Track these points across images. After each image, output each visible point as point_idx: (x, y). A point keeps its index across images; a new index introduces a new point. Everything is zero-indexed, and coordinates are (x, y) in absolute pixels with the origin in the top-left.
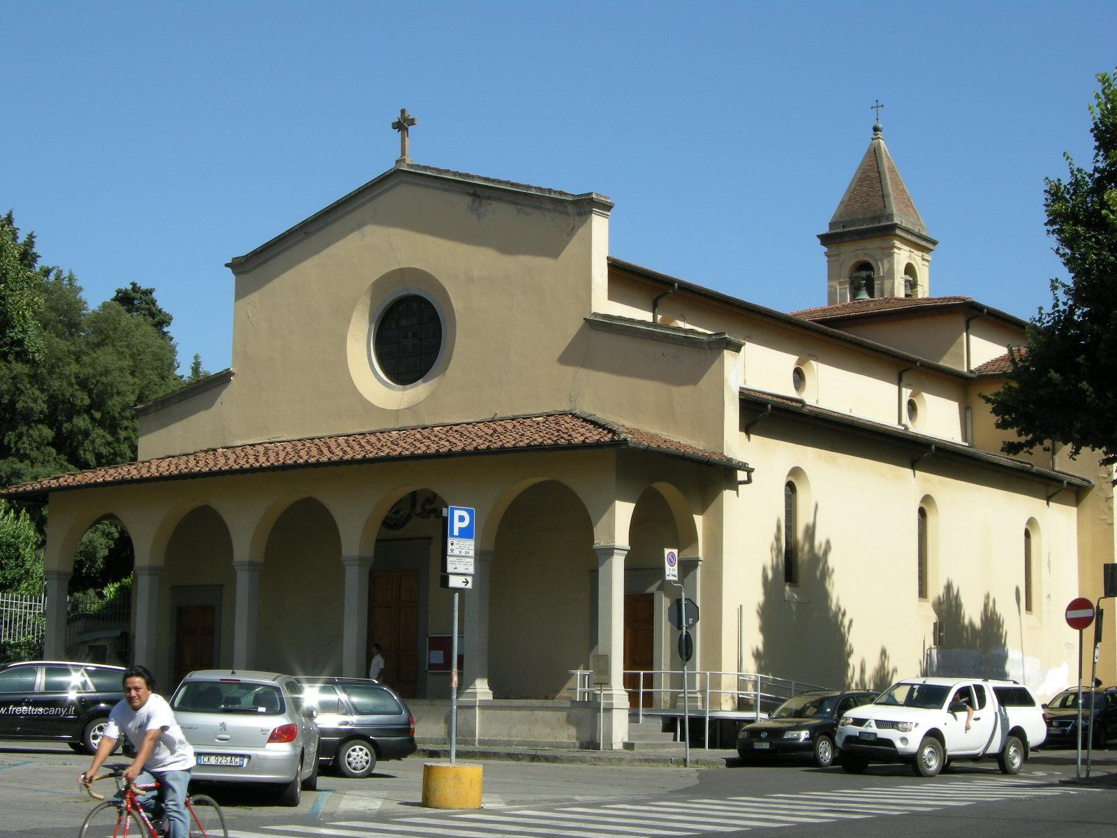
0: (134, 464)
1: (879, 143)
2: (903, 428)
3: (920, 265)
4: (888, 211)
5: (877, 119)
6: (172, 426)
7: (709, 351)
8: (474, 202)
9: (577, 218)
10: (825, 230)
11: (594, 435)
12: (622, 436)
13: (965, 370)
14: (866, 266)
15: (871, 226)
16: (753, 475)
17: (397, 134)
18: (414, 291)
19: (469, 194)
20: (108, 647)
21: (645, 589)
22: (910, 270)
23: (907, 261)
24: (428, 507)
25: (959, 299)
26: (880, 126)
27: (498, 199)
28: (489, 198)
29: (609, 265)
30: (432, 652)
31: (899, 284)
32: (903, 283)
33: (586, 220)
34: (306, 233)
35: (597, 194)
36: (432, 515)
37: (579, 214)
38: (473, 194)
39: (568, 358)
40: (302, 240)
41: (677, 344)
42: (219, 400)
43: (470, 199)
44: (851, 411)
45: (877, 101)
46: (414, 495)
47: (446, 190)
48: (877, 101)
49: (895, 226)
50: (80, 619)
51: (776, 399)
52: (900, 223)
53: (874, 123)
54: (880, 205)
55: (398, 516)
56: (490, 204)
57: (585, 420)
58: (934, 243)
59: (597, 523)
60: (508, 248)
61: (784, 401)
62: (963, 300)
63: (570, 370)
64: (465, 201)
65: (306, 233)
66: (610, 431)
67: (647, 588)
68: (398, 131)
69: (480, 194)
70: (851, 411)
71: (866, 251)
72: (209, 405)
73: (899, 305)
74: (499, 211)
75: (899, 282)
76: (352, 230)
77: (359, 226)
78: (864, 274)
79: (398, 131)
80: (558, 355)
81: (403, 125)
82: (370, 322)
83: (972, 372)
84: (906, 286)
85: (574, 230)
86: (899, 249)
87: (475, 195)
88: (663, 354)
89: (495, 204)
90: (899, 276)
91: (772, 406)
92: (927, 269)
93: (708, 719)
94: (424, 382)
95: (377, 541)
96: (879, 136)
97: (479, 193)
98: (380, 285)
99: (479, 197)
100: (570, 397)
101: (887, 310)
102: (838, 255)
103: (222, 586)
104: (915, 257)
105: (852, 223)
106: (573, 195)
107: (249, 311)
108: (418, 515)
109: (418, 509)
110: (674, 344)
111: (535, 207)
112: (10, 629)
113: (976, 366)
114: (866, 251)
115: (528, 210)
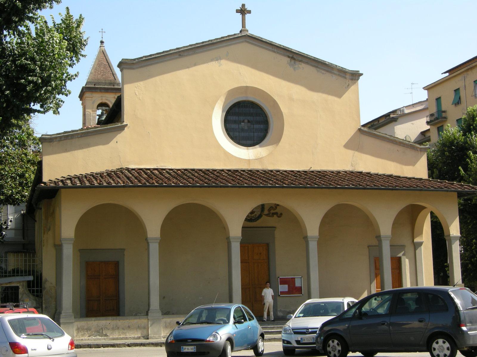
5: (102, 38)
6: (76, 151)
7: (419, 152)
8: (291, 61)
9: (350, 81)
15: (110, 87)
17: (239, 16)
18: (251, 98)
19: (289, 57)
20: (20, 287)
21: (397, 255)
24: (272, 211)
26: (104, 41)
27: (307, 63)
28: (300, 61)
30: (300, 286)
33: (355, 83)
34: (180, 55)
37: (352, 79)
38: (292, 57)
39: (349, 145)
40: (176, 58)
41: (405, 147)
42: (115, 140)
43: (289, 59)
46: (263, 206)
47: (274, 52)
50: (14, 270)
53: (101, 39)
55: (253, 215)
56: (301, 64)
59: (451, 225)
60: (312, 88)
63: (350, 152)
64: (285, 60)
65: (180, 55)
67: (399, 254)
68: (241, 14)
69: (296, 58)
71: (107, 98)
72: (107, 142)
74: (306, 69)
76: (212, 60)
77: (218, 59)
79: (241, 14)
80: (344, 144)
81: (243, 11)
82: (223, 111)
85: (348, 86)
87: (292, 58)
88: (398, 150)
89: (303, 65)
94: (260, 147)
95: (243, 227)
97: (295, 57)
98: (232, 92)
99: (294, 59)
100: (352, 164)
102: (92, 97)
103: (124, 249)
105: (99, 83)
107: (136, 91)
108: (267, 215)
109: (266, 212)
110: (403, 146)
111: (328, 71)
114: (107, 98)
115: (323, 72)
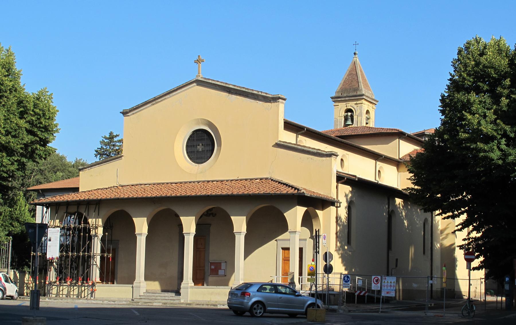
0: (78, 193)
1: (356, 59)
2: (377, 182)
3: (371, 110)
4: (360, 88)
10: (334, 95)
11: (291, 191)
12: (302, 191)
13: (398, 158)
14: (350, 110)
16: (341, 204)
22: (368, 112)
23: (367, 109)
25: (396, 130)
29: (285, 122)
31: (364, 119)
32: (365, 118)
35: (281, 95)
36: (211, 215)
44: (393, 185)
45: (356, 42)
48: (356, 42)
49: (363, 95)
51: (348, 176)
52: (365, 94)
54: (357, 86)
57: (279, 183)
58: (377, 101)
61: (351, 176)
62: (398, 131)
66: (296, 189)
70: (393, 185)
73: (374, 131)
75: (364, 118)
78: (349, 114)
83: (400, 159)
84: (366, 119)
86: (364, 104)
90: (364, 115)
91: (347, 178)
92: (374, 112)
93: (375, 298)
96: (356, 56)
101: (367, 133)
104: (370, 107)
106: (271, 95)
112: (6, 255)
113: (402, 157)
